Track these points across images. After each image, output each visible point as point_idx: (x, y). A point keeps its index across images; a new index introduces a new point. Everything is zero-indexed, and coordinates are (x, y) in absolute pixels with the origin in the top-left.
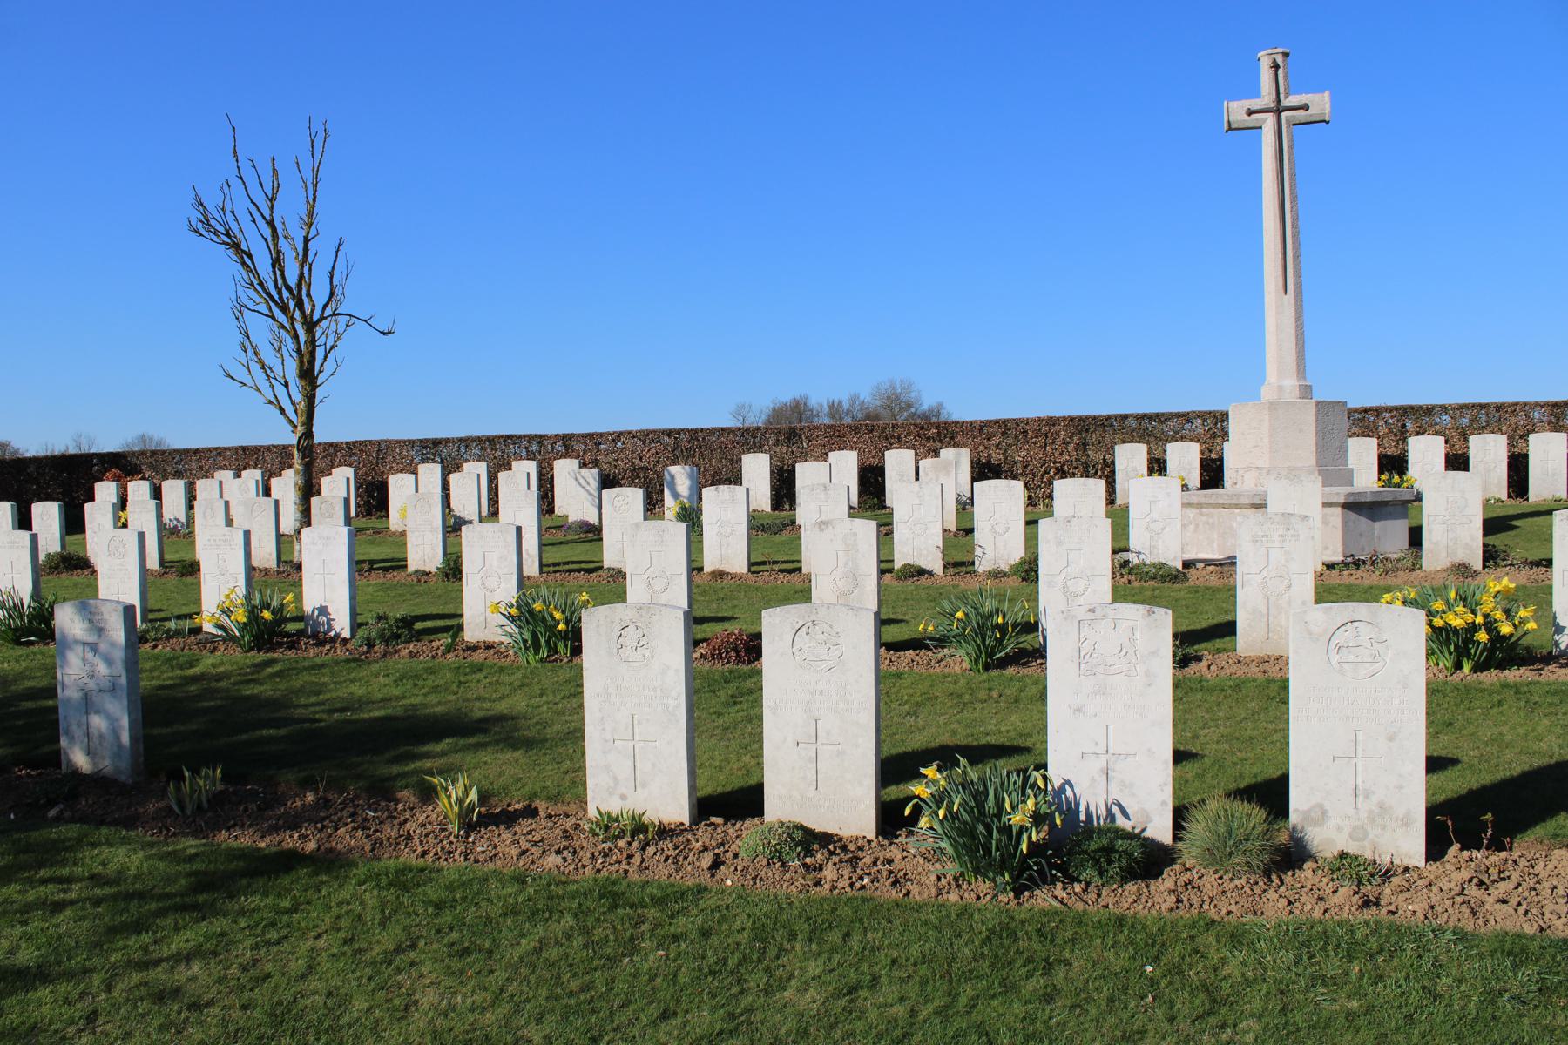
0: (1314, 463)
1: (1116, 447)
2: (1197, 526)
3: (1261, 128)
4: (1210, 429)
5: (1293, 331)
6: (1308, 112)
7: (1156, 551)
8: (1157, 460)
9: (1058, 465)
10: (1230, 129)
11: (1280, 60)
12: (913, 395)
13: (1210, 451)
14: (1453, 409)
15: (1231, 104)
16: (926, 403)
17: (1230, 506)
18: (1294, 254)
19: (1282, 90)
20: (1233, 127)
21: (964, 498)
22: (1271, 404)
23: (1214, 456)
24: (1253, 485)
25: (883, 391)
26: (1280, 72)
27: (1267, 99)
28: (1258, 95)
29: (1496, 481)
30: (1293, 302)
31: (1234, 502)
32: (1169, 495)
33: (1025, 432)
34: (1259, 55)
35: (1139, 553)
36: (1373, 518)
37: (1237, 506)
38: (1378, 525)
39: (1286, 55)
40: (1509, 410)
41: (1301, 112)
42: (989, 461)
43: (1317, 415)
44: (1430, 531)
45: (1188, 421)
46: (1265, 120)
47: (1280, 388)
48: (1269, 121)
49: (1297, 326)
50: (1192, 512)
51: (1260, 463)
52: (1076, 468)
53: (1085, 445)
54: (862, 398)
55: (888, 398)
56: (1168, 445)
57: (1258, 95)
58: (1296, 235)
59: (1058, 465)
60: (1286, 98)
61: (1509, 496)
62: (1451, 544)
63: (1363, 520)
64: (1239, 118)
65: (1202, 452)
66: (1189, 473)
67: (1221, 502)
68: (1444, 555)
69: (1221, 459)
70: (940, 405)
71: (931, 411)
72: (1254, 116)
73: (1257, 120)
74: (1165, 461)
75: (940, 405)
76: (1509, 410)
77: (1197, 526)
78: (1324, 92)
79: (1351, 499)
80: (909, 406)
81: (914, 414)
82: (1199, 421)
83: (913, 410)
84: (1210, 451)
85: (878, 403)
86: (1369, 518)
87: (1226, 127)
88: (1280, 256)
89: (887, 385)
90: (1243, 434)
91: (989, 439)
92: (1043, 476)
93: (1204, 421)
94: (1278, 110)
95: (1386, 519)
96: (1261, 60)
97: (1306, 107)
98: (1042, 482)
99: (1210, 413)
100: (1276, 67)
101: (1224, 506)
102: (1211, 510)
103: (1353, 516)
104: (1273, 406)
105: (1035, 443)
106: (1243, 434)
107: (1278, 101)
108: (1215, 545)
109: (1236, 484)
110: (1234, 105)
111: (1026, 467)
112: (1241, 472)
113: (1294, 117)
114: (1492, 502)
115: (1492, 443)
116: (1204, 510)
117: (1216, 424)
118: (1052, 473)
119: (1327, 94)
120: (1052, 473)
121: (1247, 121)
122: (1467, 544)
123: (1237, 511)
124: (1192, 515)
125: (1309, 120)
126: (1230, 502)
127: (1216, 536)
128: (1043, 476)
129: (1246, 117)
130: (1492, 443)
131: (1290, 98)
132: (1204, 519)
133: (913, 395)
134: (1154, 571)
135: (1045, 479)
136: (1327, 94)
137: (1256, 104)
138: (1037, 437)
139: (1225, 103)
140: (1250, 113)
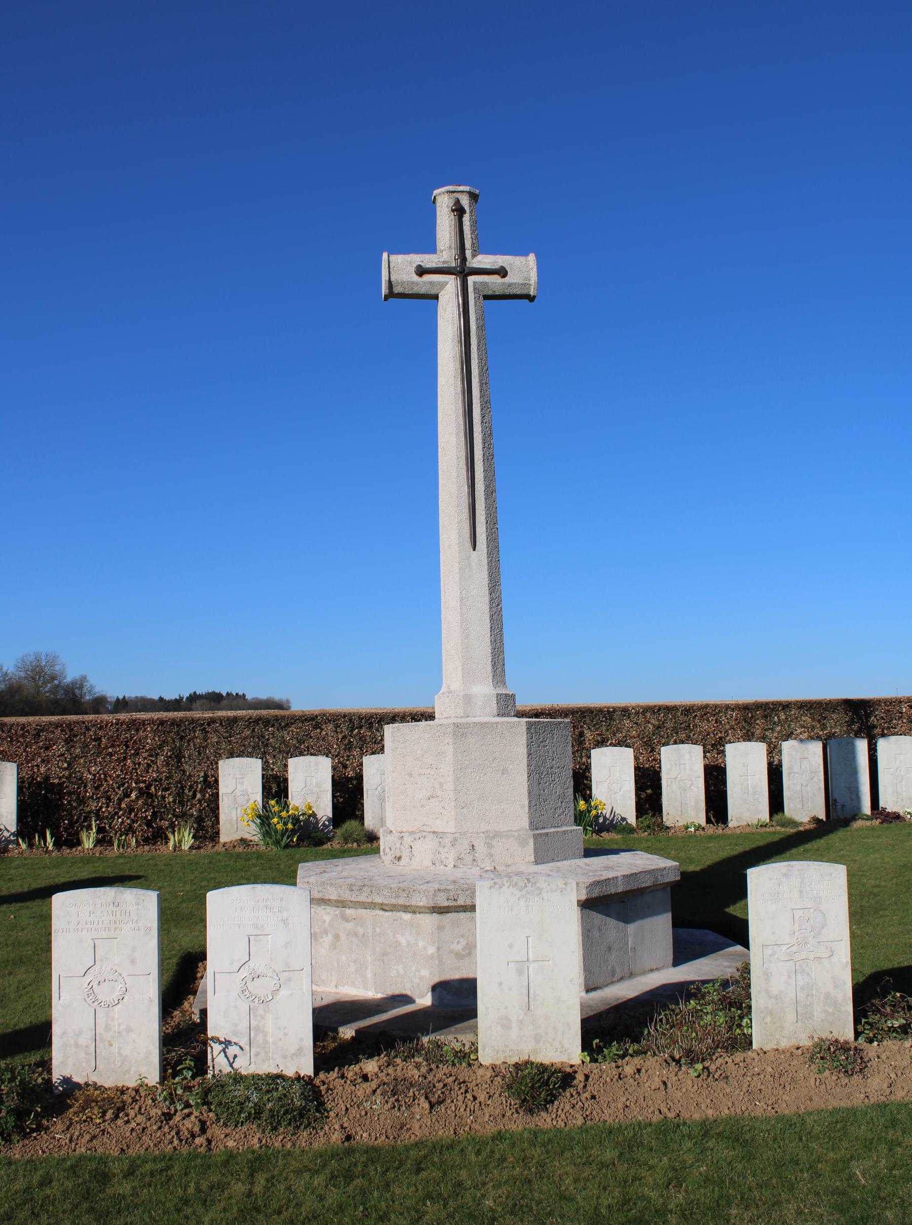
0: (525, 822)
1: (221, 763)
2: (337, 937)
3: (436, 297)
4: (344, 737)
5: (486, 608)
6: (507, 280)
7: (260, 1038)
8: (275, 777)
9: (142, 785)
10: (391, 294)
11: (465, 201)
12: (57, 668)
13: (345, 767)
14: (637, 713)
15: (393, 258)
16: (71, 675)
17: (394, 908)
18: (487, 487)
19: (468, 244)
20: (397, 290)
21: (6, 834)
22: (457, 726)
23: (350, 773)
24: (427, 863)
25: (28, 663)
26: (466, 219)
27: (445, 254)
28: (432, 249)
29: (693, 803)
30: (485, 562)
31: (401, 901)
32: (285, 922)
33: (98, 739)
34: (436, 192)
35: (228, 1043)
36: (626, 918)
37: (406, 909)
38: (631, 928)
39: (474, 197)
40: (698, 714)
41: (495, 279)
42: (47, 778)
43: (529, 745)
44: (767, 975)
45: (316, 727)
46: (443, 285)
47: (468, 699)
48: (449, 287)
49: (492, 600)
50: (327, 914)
51: (439, 826)
52: (166, 789)
53: (179, 757)
54: (5, 669)
55: (33, 670)
56: (290, 760)
57: (432, 249)
58: (489, 459)
59: (142, 785)
60: (474, 256)
61: (708, 821)
62: (801, 996)
63: (612, 922)
64: (406, 278)
65: (334, 768)
66: (318, 798)
67: (379, 900)
68: (791, 1017)
69: (359, 778)
70: (84, 679)
71: (74, 683)
72: (428, 278)
73: (431, 283)
74: (286, 780)
75: (84, 679)
76: (698, 714)
77: (337, 937)
78: (527, 255)
79: (596, 893)
80: (53, 678)
81: (58, 686)
82: (331, 726)
83: (56, 682)
84: (345, 767)
85: (23, 674)
86: (619, 919)
87: (384, 290)
88: (465, 489)
89: (32, 658)
90: (410, 775)
91: (47, 748)
92: (120, 800)
93: (337, 726)
94: (463, 272)
95: (643, 916)
96: (439, 199)
97: (502, 272)
98: (120, 809)
99: (345, 716)
100: (459, 211)
101: (383, 908)
102: (362, 912)
103: (597, 918)
104: (460, 730)
105: (111, 755)
106: (410, 775)
107: (464, 259)
108: (369, 975)
109: (399, 858)
110: (398, 260)
111: (97, 788)
112: (408, 839)
113: (485, 284)
114: (692, 829)
115: (687, 756)
116: (348, 911)
117: (352, 731)
118: (133, 796)
119: (532, 257)
120: (133, 796)
121: (417, 284)
122: (828, 995)
123: (407, 916)
124: (327, 918)
125: (507, 292)
126: (393, 901)
127: (369, 958)
128: (120, 800)
129: (416, 278)
130: (687, 756)
131: (480, 257)
132: (350, 926)
133: (57, 668)
134: (255, 1098)
135: (123, 806)
136: (532, 257)
137: (429, 261)
138: (113, 746)
139: (385, 255)
140: (421, 271)
